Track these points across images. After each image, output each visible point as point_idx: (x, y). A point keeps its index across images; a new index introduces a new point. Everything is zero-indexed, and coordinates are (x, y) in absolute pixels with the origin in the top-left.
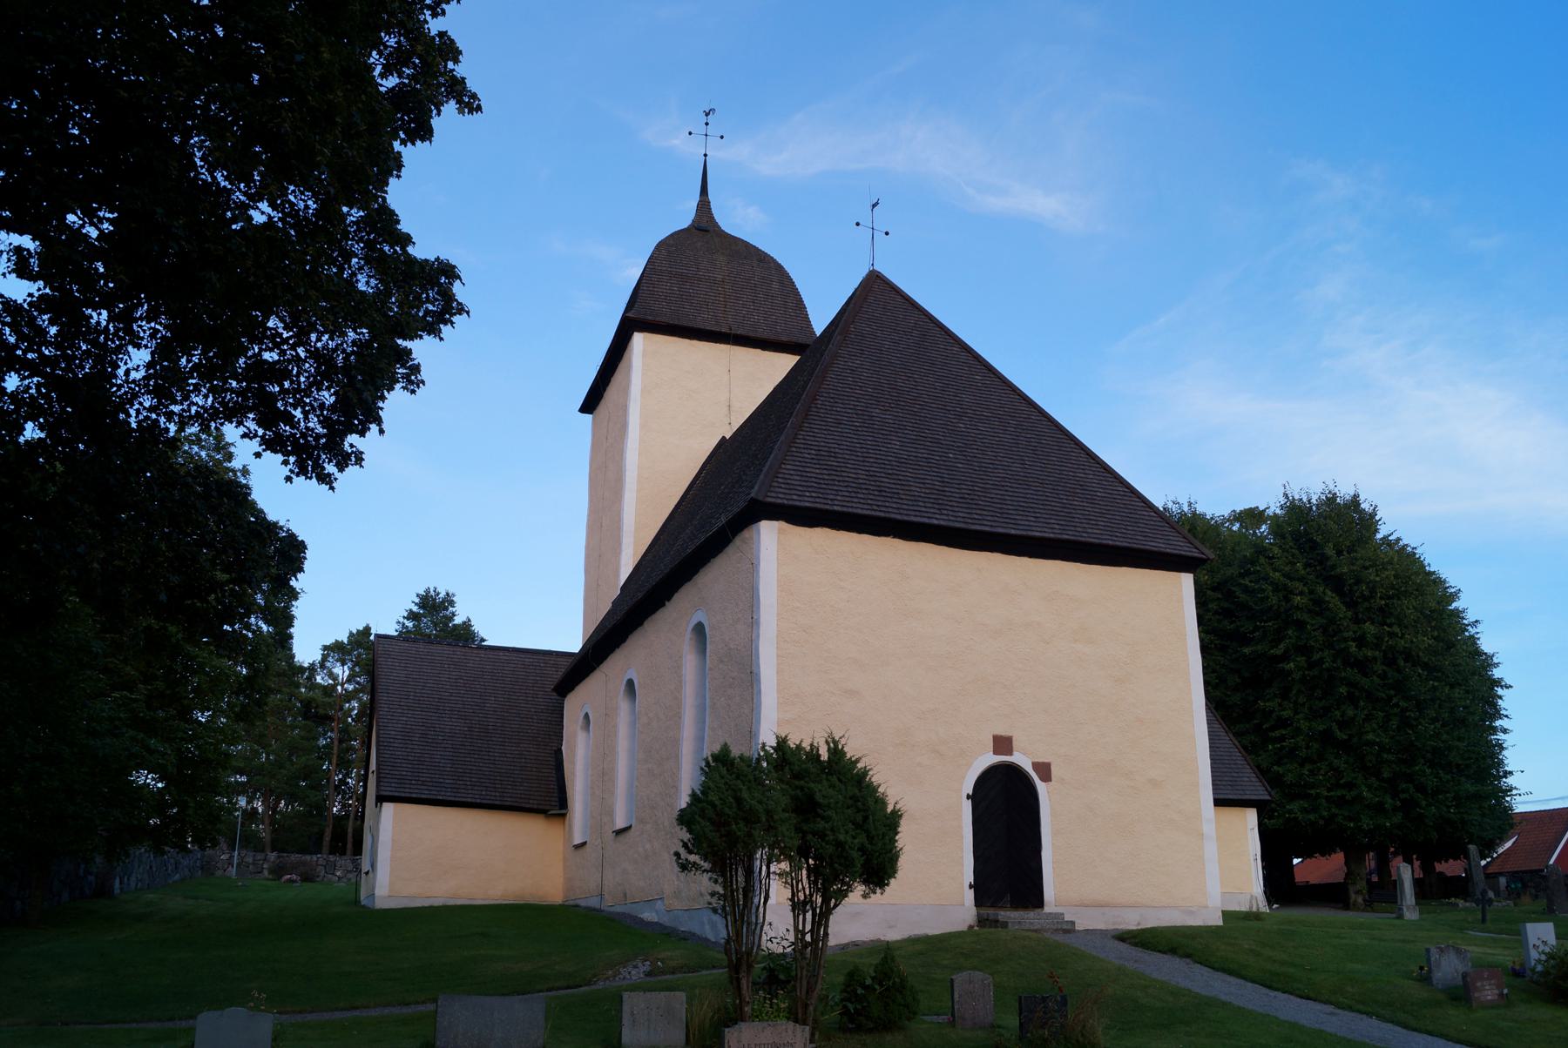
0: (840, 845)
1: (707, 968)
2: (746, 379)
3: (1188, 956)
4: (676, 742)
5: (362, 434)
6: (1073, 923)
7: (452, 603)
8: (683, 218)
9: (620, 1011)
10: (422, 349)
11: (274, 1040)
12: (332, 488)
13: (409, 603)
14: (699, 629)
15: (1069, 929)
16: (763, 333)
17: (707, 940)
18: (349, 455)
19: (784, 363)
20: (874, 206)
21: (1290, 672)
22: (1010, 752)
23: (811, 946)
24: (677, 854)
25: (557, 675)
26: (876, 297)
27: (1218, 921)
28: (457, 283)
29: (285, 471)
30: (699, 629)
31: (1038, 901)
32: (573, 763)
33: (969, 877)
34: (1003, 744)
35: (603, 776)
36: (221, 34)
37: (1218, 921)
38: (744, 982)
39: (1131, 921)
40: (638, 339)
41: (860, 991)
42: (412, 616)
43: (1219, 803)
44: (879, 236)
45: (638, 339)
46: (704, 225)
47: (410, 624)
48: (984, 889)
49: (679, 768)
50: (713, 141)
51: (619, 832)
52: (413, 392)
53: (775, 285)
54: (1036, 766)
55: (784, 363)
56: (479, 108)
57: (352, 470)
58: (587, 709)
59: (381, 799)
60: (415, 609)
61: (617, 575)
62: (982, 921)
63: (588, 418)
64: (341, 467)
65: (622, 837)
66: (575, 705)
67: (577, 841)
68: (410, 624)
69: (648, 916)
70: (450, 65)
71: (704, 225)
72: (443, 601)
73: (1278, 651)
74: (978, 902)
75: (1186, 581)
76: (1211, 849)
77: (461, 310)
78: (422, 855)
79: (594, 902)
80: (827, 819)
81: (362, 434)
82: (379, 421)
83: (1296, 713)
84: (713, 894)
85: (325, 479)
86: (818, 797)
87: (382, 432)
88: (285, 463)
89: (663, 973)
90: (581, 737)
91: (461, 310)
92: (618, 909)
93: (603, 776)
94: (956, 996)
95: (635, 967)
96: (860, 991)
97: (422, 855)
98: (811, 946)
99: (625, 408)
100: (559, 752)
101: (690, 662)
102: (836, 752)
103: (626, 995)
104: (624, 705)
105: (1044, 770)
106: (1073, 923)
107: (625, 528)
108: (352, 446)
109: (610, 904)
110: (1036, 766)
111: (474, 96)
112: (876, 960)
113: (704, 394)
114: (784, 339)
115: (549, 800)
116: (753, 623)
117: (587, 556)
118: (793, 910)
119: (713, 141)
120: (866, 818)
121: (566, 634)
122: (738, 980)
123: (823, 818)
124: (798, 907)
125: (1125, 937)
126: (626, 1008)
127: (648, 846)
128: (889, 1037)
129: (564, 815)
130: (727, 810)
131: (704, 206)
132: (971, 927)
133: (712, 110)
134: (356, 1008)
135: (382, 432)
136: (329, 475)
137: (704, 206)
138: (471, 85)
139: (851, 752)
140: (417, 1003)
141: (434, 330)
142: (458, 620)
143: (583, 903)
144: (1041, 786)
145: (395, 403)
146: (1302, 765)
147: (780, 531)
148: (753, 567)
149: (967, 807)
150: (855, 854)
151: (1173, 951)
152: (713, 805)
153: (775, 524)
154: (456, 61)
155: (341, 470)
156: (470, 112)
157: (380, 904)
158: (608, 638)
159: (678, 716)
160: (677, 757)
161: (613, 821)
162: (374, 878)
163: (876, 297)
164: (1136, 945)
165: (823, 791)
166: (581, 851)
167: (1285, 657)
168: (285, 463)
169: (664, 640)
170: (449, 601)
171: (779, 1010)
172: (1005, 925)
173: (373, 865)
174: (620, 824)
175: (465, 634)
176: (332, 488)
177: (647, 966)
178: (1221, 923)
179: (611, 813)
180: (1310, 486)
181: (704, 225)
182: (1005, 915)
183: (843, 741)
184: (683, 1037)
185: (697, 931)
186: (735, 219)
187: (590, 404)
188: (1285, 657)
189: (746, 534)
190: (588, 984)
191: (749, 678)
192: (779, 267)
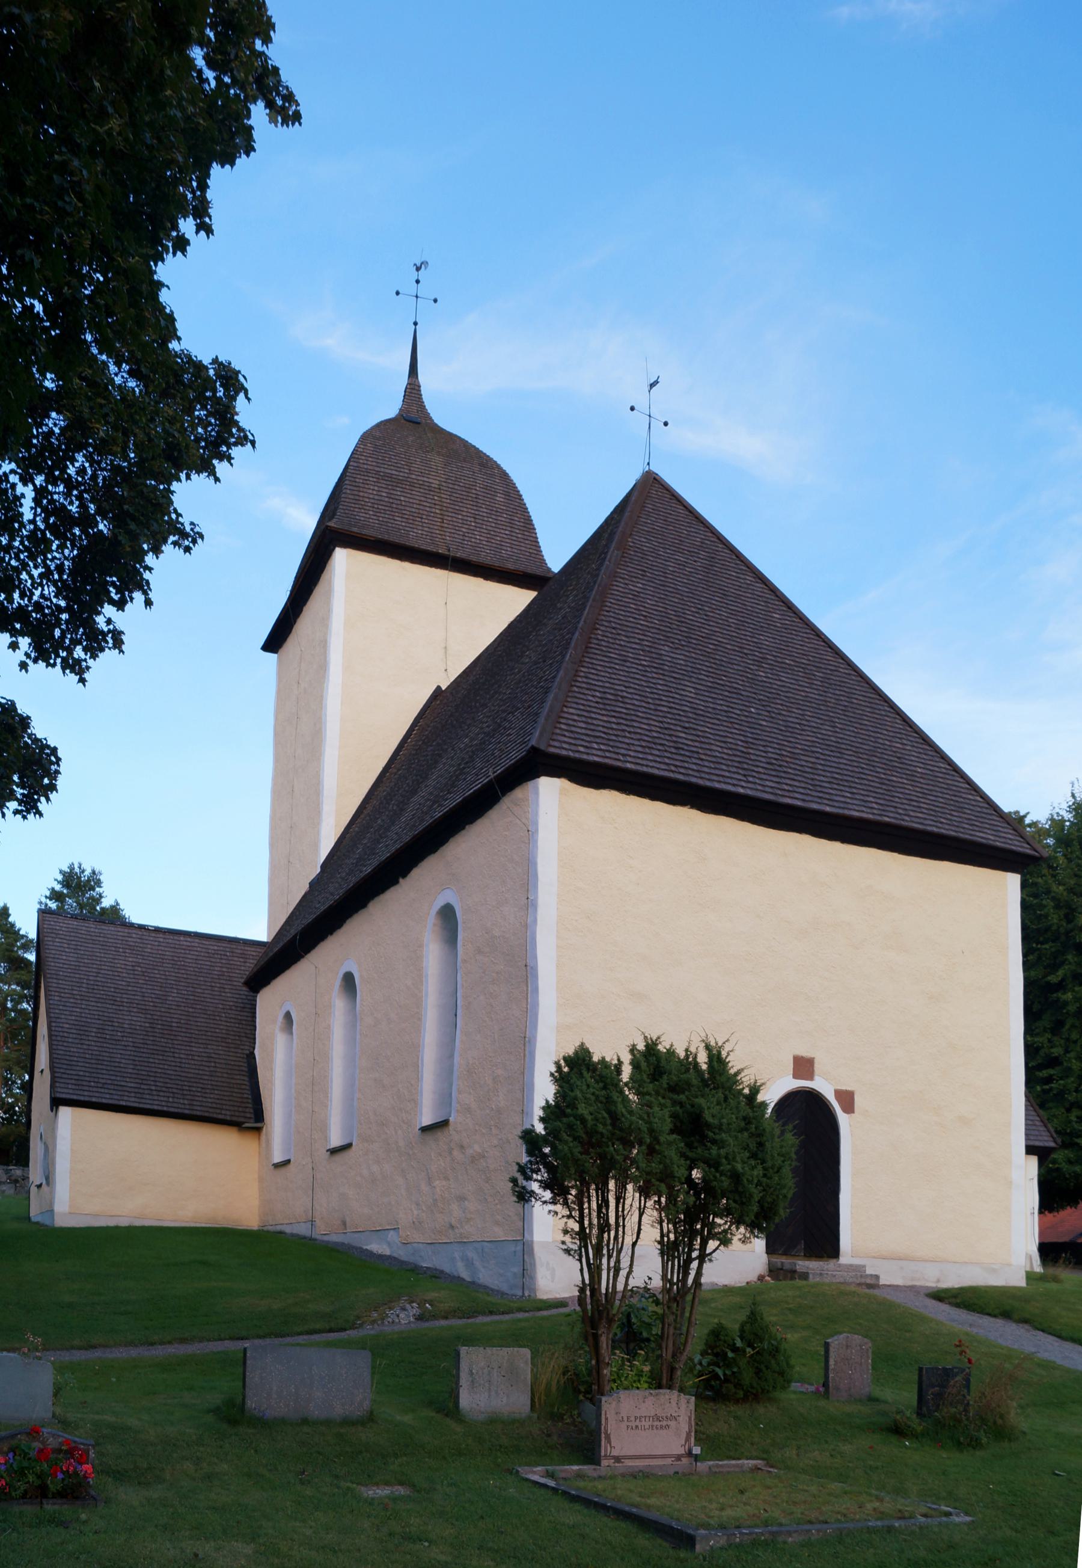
0: (736, 1177)
1: (484, 1314)
2: (465, 618)
3: (1025, 1321)
4: (416, 1048)
5: (120, 605)
6: (877, 1277)
7: (99, 883)
8: (390, 408)
9: (458, 1369)
10: (189, 496)
11: (55, 1395)
12: (82, 681)
13: (51, 880)
14: (447, 914)
15: (873, 1284)
16: (486, 557)
17: (459, 1279)
18: (104, 634)
19: (512, 602)
20: (652, 385)
21: (1066, 1003)
22: (810, 1076)
23: (680, 1294)
24: (514, 1181)
25: (249, 967)
26: (652, 514)
27: (1022, 1283)
28: (241, 396)
29: (19, 655)
30: (447, 914)
32: (271, 1069)
35: (312, 1084)
37: (1022, 1283)
38: (603, 1339)
39: (953, 1280)
40: (342, 558)
41: (730, 1355)
42: (55, 895)
44: (657, 425)
45: (342, 558)
46: (413, 419)
47: (53, 905)
49: (419, 1078)
51: (334, 1151)
52: (187, 550)
53: (500, 498)
54: (839, 1094)
55: (512, 602)
56: (297, 117)
57: (108, 656)
58: (288, 1007)
59: (56, 1103)
60: (58, 887)
61: (316, 846)
62: (774, 1271)
63: (272, 657)
64: (94, 651)
65: (338, 1158)
66: (270, 1003)
67: (278, 1158)
68: (53, 905)
69: (376, 1247)
70: (258, 45)
71: (413, 415)
72: (89, 881)
73: (1053, 979)
75: (1012, 882)
77: (245, 439)
78: (106, 1168)
79: (303, 1230)
80: (721, 1144)
81: (120, 605)
82: (143, 587)
83: (1067, 1051)
84: (566, 1232)
85: (77, 668)
86: (707, 1116)
87: (148, 603)
88: (14, 646)
89: (434, 1317)
90: (281, 1040)
91: (245, 439)
92: (334, 1238)
93: (312, 1084)
94: (832, 1362)
95: (404, 1309)
96: (730, 1355)
97: (106, 1168)
98: (680, 1294)
99: (324, 644)
100: (251, 1057)
101: (433, 953)
102: (717, 1059)
103: (463, 1350)
104: (339, 1004)
105: (847, 1099)
106: (877, 1277)
107: (326, 793)
108: (109, 622)
109: (324, 1230)
110: (839, 1094)
111: (290, 97)
112: (742, 1316)
113: (415, 633)
114: (510, 566)
115: (244, 1112)
116: (529, 905)
117: (273, 827)
118: (662, 1254)
120: (761, 1145)
121: (249, 916)
122: (596, 1337)
123: (714, 1142)
124: (668, 1250)
125: (940, 1296)
126: (464, 1366)
127: (375, 1168)
128: (761, 1410)
129: (259, 1130)
130: (600, 1128)
131: (413, 391)
132: (761, 1278)
133: (424, 263)
134: (94, 1347)
135: (148, 603)
136: (78, 661)
137: (413, 391)
138: (287, 77)
139: (735, 1063)
140: (162, 1343)
141: (206, 467)
142: (106, 903)
143: (288, 1230)
144: (842, 1118)
145: (165, 567)
146: (1068, 1110)
147: (563, 792)
148: (529, 835)
150: (752, 1188)
151: (1006, 1315)
152: (583, 1121)
154: (267, 40)
155: (94, 657)
156: (285, 122)
157: (60, 1222)
158: (318, 919)
159: (416, 1018)
160: (416, 1067)
161: (326, 1139)
162: (52, 1193)
163: (652, 514)
164: (958, 1305)
165: (710, 1108)
166: (283, 1171)
167: (1061, 986)
168: (14, 646)
169: (395, 930)
170: (94, 881)
171: (640, 1374)
172: (804, 1276)
173: (49, 1178)
174: (335, 1141)
175: (113, 915)
176: (82, 681)
177: (414, 1310)
179: (324, 1128)
181: (413, 419)
182: (803, 1265)
183: (728, 1047)
184: (529, 1402)
185: (447, 1268)
186: (444, 414)
187: (275, 642)
188: (1061, 986)
189: (518, 793)
190: (353, 1327)
191: (524, 973)
192: (504, 476)
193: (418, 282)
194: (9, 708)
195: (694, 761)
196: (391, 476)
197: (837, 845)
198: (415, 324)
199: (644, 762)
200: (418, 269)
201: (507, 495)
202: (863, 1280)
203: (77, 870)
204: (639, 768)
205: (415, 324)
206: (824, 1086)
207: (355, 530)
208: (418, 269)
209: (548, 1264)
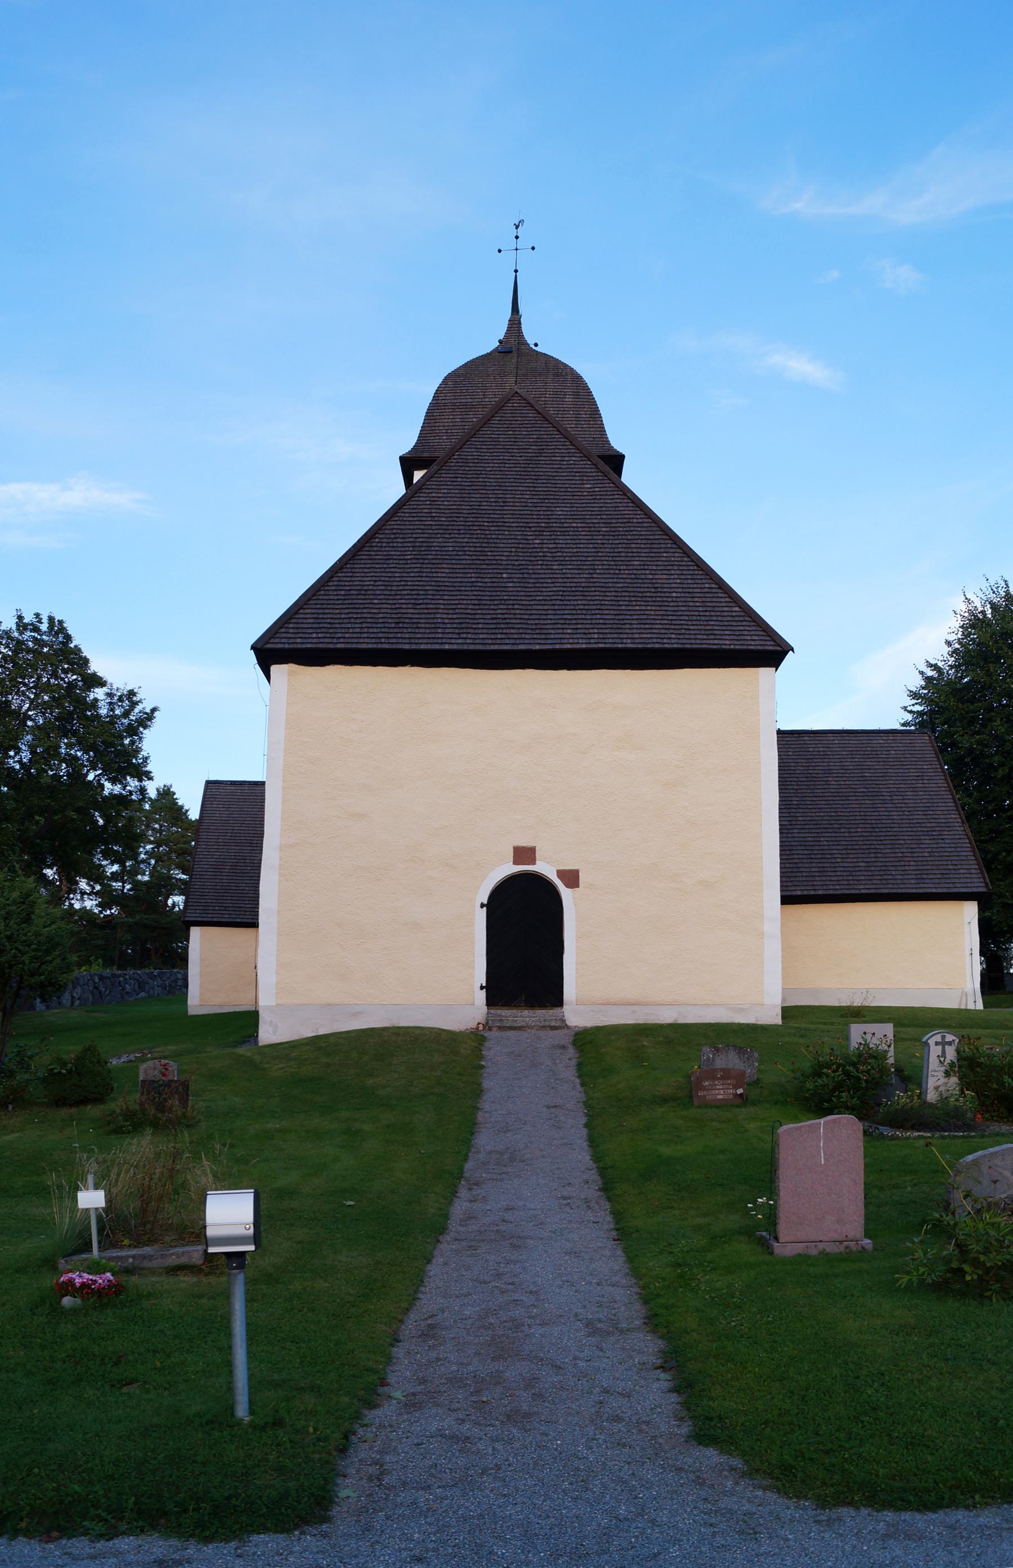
22: (533, 861)
27: (774, 1018)
31: (556, 999)
33: (482, 978)
34: (524, 854)
36: (835, 274)
37: (774, 1018)
43: (787, 900)
46: (513, 346)
48: (501, 989)
50: (525, 255)
54: (562, 874)
74: (490, 1002)
76: (773, 950)
105: (571, 878)
110: (562, 874)
119: (525, 255)
133: (521, 221)
147: (291, 674)
149: (480, 918)
153: (285, 667)
178: (778, 1020)
180: (88, 657)
181: (513, 346)
193: (517, 237)
194: (50, 654)
195: (365, 635)
196: (466, 404)
197: (564, 673)
198: (516, 271)
199: (353, 640)
200: (517, 227)
201: (576, 395)
202: (547, 1023)
203: (930, 673)
204: (349, 646)
205: (516, 271)
206: (546, 868)
207: (426, 455)
208: (517, 227)
209: (271, 1022)
